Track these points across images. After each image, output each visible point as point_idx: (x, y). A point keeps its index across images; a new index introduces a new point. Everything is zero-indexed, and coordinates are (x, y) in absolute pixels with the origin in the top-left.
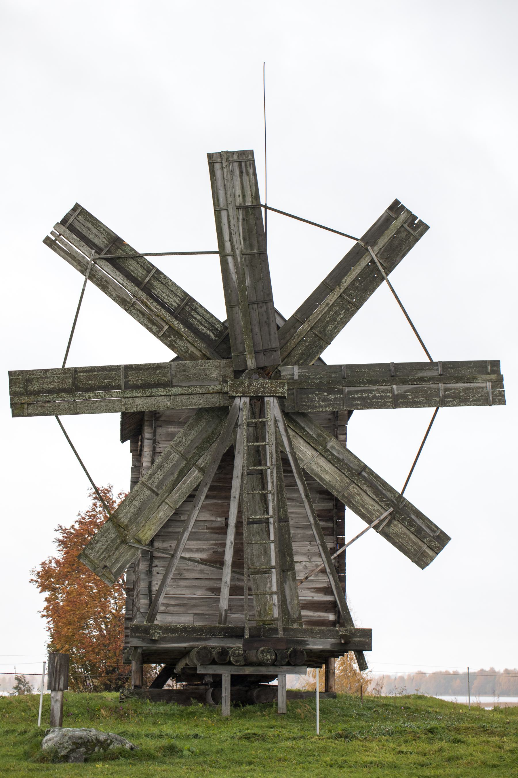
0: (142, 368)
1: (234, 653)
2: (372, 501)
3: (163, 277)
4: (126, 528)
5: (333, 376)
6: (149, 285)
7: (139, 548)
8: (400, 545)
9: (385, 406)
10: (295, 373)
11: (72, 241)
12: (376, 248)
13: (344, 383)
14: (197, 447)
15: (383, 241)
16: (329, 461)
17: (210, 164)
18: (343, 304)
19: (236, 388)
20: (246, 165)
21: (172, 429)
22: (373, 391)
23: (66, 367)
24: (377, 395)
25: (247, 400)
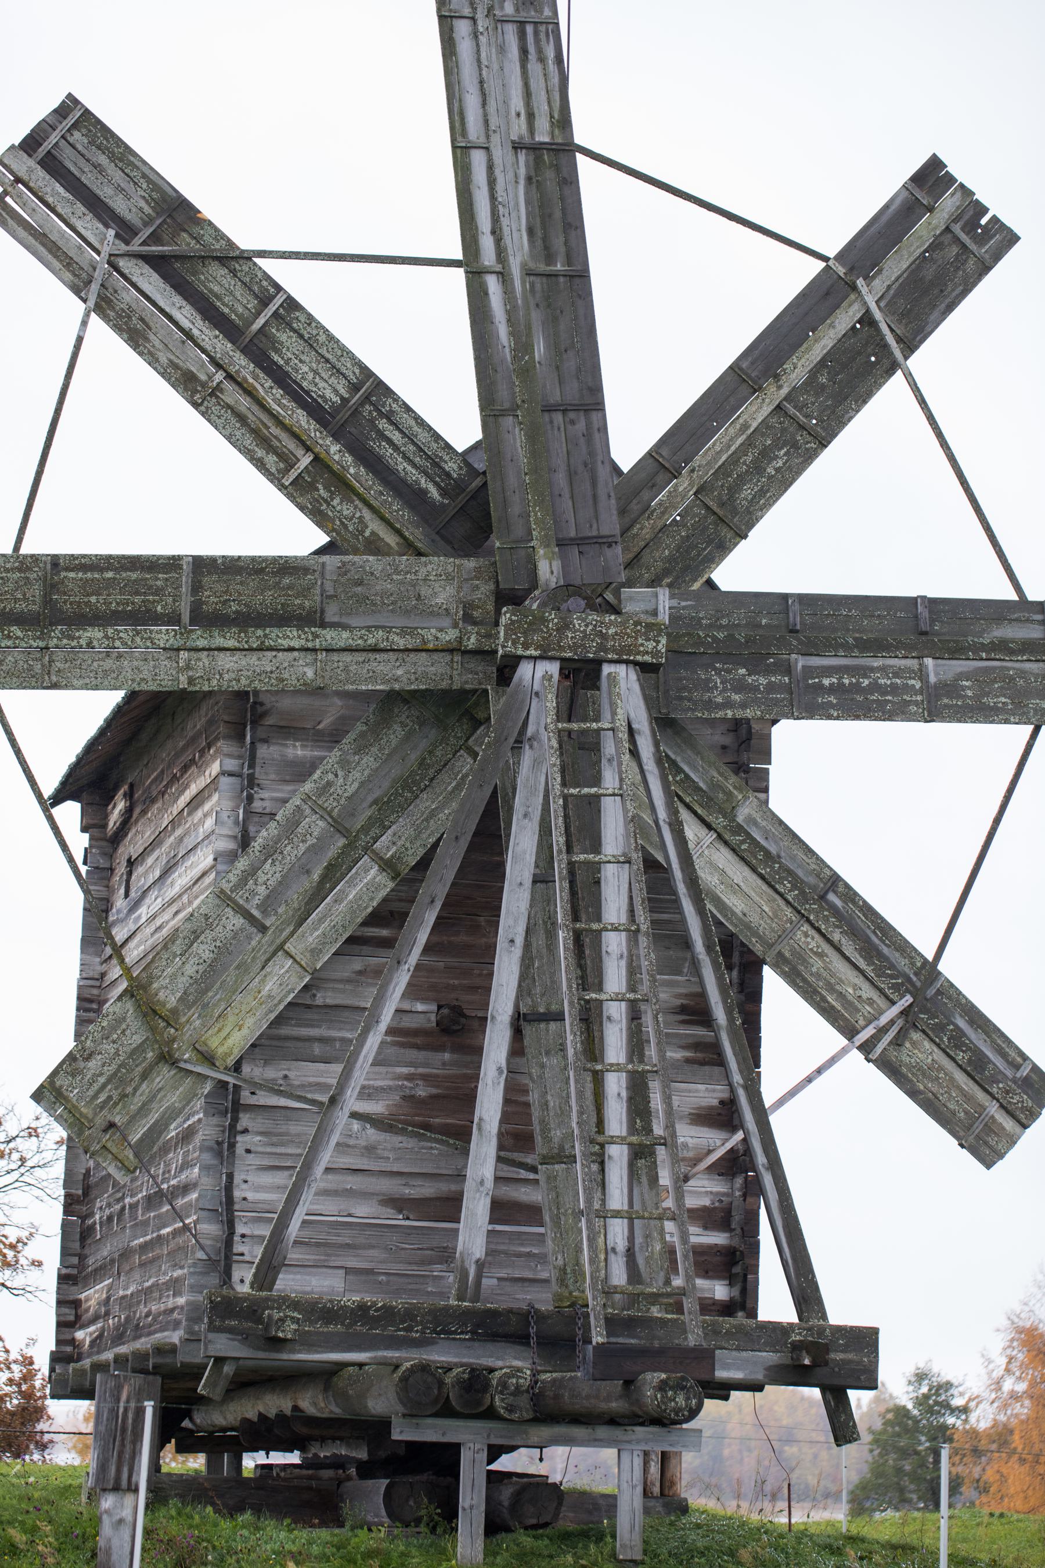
0: (242, 568)
1: (503, 1384)
2: (856, 973)
3: (302, 318)
4: (171, 1019)
5: (764, 621)
6: (263, 339)
7: (207, 1077)
8: (929, 1100)
9: (903, 713)
10: (661, 608)
11: (50, 200)
12: (877, 282)
13: (795, 643)
14: (375, 802)
15: (896, 266)
16: (742, 859)
17: (441, 18)
18: (784, 430)
19: (525, 633)
20: (536, 33)
21: (297, 751)
22: (872, 669)
23: (24, 550)
24: (882, 681)
25: (553, 668)
